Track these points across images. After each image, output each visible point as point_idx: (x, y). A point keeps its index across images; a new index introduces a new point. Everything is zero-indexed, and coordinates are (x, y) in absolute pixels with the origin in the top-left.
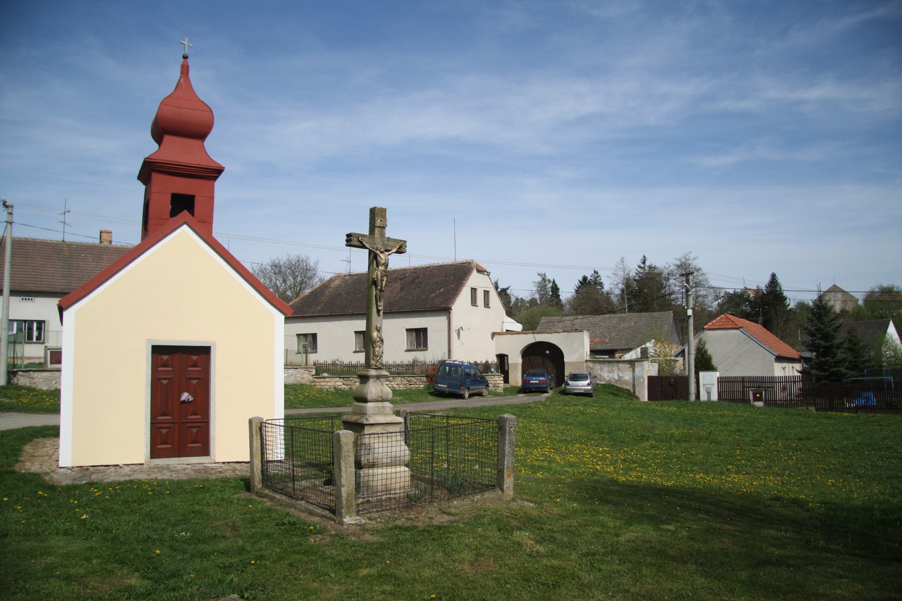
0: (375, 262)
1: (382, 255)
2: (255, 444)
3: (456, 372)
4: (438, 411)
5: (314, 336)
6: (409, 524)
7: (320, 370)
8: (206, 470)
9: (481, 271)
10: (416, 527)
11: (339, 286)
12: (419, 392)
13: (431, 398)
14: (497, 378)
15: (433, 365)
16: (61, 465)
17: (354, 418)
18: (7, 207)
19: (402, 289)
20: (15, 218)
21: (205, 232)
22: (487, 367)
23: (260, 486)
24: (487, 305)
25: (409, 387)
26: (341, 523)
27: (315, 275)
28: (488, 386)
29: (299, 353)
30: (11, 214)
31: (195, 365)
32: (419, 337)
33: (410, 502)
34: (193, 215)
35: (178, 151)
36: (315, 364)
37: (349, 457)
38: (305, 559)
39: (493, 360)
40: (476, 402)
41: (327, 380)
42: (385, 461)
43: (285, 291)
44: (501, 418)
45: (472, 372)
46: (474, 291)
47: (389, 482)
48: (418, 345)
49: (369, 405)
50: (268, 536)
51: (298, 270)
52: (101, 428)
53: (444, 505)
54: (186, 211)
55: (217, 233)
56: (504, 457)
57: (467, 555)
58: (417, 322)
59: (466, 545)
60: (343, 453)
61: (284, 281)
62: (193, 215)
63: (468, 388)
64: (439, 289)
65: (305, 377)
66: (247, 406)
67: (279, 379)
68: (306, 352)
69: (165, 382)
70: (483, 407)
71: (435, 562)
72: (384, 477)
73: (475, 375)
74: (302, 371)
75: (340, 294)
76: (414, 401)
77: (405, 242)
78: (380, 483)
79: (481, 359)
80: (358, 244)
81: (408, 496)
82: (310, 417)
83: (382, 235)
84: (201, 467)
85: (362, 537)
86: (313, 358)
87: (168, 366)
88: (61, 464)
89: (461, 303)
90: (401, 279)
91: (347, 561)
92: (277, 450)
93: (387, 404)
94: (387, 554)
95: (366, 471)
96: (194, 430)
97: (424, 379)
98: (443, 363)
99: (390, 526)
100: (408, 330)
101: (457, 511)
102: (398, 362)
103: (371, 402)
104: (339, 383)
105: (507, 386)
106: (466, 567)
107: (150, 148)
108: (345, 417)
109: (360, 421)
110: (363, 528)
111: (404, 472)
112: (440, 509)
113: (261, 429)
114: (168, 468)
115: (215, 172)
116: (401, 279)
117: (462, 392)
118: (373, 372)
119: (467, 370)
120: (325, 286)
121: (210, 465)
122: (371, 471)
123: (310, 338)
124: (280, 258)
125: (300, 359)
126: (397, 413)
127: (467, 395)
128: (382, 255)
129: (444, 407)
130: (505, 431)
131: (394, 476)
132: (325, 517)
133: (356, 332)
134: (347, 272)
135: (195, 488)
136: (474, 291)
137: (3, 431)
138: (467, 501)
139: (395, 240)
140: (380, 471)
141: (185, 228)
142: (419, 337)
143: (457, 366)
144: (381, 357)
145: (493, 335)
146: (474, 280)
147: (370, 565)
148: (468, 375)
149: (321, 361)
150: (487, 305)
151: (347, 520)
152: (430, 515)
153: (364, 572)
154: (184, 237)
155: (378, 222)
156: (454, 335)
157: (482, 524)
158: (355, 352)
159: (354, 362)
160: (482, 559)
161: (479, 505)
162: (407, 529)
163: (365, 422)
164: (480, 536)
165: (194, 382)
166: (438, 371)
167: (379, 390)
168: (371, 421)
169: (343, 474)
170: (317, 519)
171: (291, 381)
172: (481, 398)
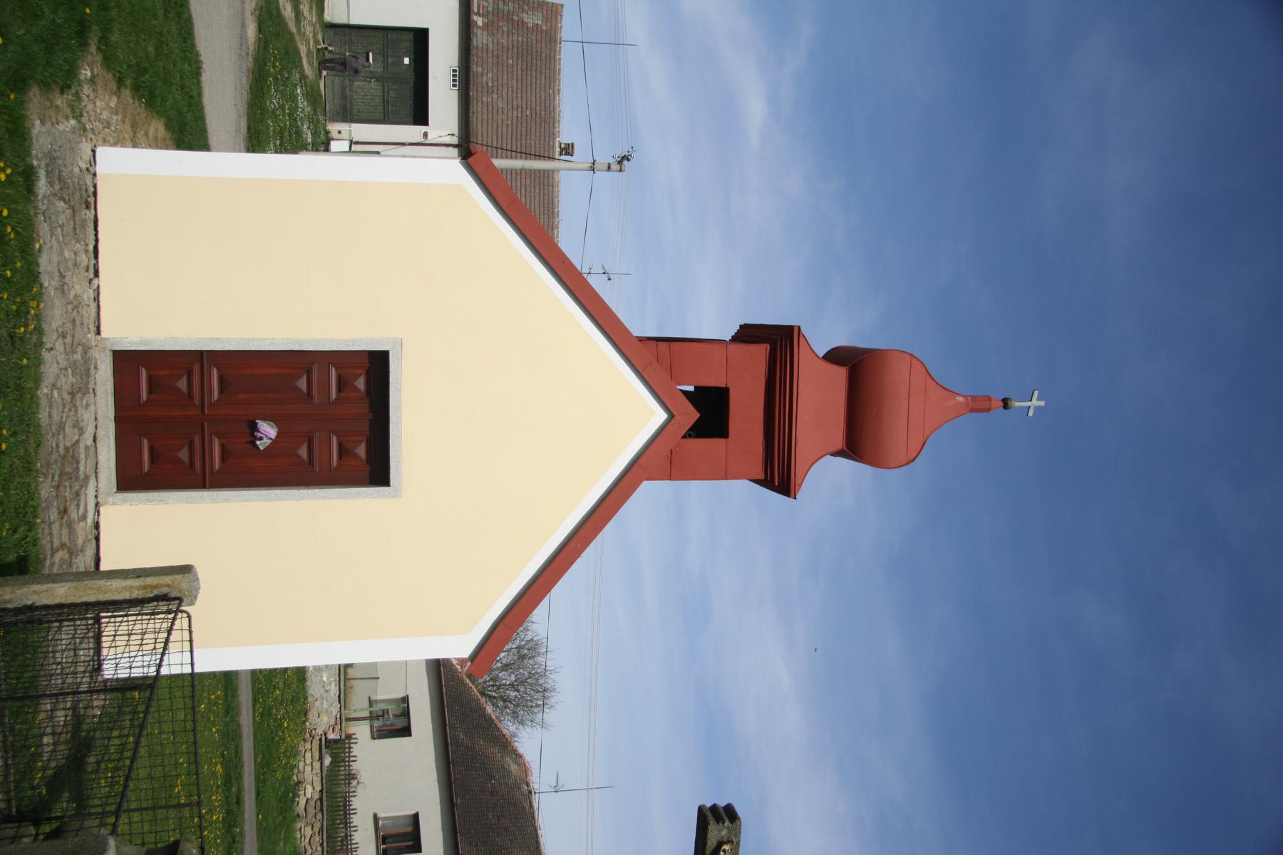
5: (406, 731)
7: (338, 749)
8: (72, 475)
11: (507, 773)
16: (100, 150)
18: (620, 163)
20: (600, 175)
21: (652, 463)
27: (522, 723)
29: (371, 703)
30: (609, 168)
31: (343, 451)
34: (684, 437)
35: (819, 399)
36: (349, 737)
41: (317, 765)
51: (529, 693)
52: (189, 242)
54: (696, 415)
55: (650, 492)
62: (684, 437)
65: (322, 717)
66: (254, 586)
68: (372, 717)
69: (302, 384)
75: (491, 777)
82: (232, 735)
86: (362, 731)
87: (339, 390)
88: (102, 152)
92: (127, 653)
96: (184, 454)
103: (364, 719)
104: (310, 790)
107: (822, 336)
114: (83, 388)
115: (779, 476)
120: (505, 745)
121: (91, 491)
123: (400, 723)
125: (359, 706)
133: (416, 816)
134: (535, 786)
141: (660, 416)
149: (356, 750)
154: (640, 415)
158: (376, 818)
159: (356, 820)
165: (303, 452)
171: (314, 689)
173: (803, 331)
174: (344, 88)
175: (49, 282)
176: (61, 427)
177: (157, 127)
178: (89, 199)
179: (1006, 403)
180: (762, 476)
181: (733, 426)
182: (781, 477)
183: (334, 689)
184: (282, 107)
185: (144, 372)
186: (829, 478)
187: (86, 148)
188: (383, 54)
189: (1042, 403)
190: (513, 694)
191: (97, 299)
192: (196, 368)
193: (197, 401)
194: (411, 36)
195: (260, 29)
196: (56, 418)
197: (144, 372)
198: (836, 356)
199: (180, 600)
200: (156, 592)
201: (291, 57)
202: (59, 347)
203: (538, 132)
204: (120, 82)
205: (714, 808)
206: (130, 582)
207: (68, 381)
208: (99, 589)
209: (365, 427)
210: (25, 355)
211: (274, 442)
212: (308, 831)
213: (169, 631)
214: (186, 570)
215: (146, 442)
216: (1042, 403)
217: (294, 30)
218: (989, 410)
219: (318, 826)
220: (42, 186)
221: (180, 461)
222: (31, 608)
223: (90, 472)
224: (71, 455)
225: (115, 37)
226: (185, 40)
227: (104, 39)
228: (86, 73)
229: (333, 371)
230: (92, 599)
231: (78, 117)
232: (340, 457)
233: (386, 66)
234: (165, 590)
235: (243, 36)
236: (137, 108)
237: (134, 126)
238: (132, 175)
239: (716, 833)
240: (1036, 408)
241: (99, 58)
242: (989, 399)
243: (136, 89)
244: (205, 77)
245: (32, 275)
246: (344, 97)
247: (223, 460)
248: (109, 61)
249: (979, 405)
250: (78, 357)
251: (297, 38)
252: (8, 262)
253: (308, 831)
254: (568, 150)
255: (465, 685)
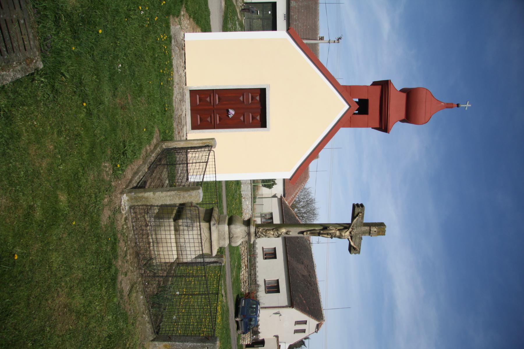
0: (342, 228)
1: (348, 233)
2: (196, 142)
3: (252, 312)
4: (226, 299)
6: (120, 252)
9: (318, 327)
10: (116, 257)
12: (239, 288)
13: (235, 295)
14: (249, 339)
15: (256, 297)
16: (186, 34)
17: (215, 214)
18: (338, 40)
19: (303, 276)
20: (332, 45)
21: (345, 122)
22: (256, 333)
23: (164, 147)
24: (296, 331)
25: (242, 282)
26: (122, 193)
28: (244, 333)
30: (334, 42)
32: (273, 288)
33: (145, 261)
35: (397, 105)
37: (179, 199)
38: (85, 150)
39: (261, 337)
40: (233, 326)
42: (182, 240)
43: (297, 208)
44: (216, 338)
45: (252, 323)
46: (305, 322)
47: (165, 245)
48: (269, 288)
49: (226, 227)
50: (114, 130)
52: (211, 58)
53: (139, 287)
55: (343, 131)
56: (182, 342)
57: (78, 301)
58: (283, 286)
59: (90, 302)
60: (182, 193)
61: (303, 207)
63: (242, 320)
64: (305, 300)
67: (245, 175)
69: (241, 98)
70: (230, 330)
71: (71, 268)
72: (169, 241)
73: (250, 324)
74: (250, 213)
76: (233, 285)
77: (359, 252)
78: (163, 236)
79: (261, 329)
80: (356, 213)
81: (151, 259)
83: (364, 233)
84: (183, 122)
85: (107, 208)
87: (252, 100)
88: (187, 35)
89: (296, 314)
90: (309, 275)
91: (80, 186)
93: (227, 242)
94: (85, 225)
95: (172, 224)
96: (209, 119)
97: (247, 292)
98: (258, 303)
99: (119, 236)
100: (278, 280)
101: (133, 298)
102: (258, 274)
105: (244, 347)
106: (63, 299)
107: (398, 84)
108: (216, 210)
109: (213, 219)
110: (117, 210)
111: (172, 256)
112: (135, 283)
113: (208, 146)
114: (182, 100)
116: (309, 275)
117: (239, 316)
118: (253, 229)
119: (254, 319)
122: (172, 228)
124: (316, 204)
126: (221, 250)
127: (237, 319)
128: (348, 233)
129: (229, 303)
130: (205, 342)
131: (169, 249)
132: (131, 181)
133: (275, 248)
135: (165, 104)
136: (305, 322)
137: (206, 4)
138: (142, 308)
139: (360, 244)
140: (173, 237)
141: (347, 107)
142: (273, 288)
143: (256, 312)
144: (265, 236)
145: (277, 337)
146: (312, 323)
147: (71, 205)
148: (251, 320)
150: (296, 331)
151: (125, 198)
152: (129, 274)
153: (63, 198)
154: (341, 107)
155: (374, 229)
156: (276, 310)
157: (117, 320)
158: (263, 248)
160: (74, 317)
161: (140, 318)
162: (114, 249)
163: (212, 223)
164: (103, 318)
165: (242, 118)
166: (253, 300)
167: (238, 235)
168: (213, 228)
169: (164, 194)
170: (129, 176)
172: (236, 329)
173: (392, 81)
174: (250, 22)
175: (175, 69)
176: (178, 109)
177: (199, 29)
178: (183, 48)
179: (458, 105)
180: (378, 126)
181: (370, 111)
182: (385, 128)
183: (250, 206)
184: (232, 27)
185: (198, 96)
186: (399, 128)
187: (182, 33)
188: (262, 11)
189: (470, 105)
190: (305, 215)
191: (185, 76)
192: (212, 95)
193: (212, 104)
194: (271, 5)
195: (226, 4)
196: (177, 106)
197: (198, 96)
198: (403, 91)
199: (212, 146)
200: (205, 144)
201: (234, 12)
202: (177, 86)
203: (312, 31)
204: (190, 16)
205: (357, 205)
206: (199, 142)
207: (179, 97)
208: (191, 143)
209: (259, 111)
210: (170, 86)
211: (234, 115)
212: (243, 248)
213: (209, 155)
214: (213, 139)
215: (199, 116)
216: (470, 105)
217: (235, 4)
218: (452, 107)
219: (246, 247)
220: (173, 41)
221: (208, 121)
222: (175, 148)
223: (185, 124)
224: (180, 117)
225: (189, 3)
226: (206, 5)
227: (186, 4)
228: (182, 13)
229: (250, 95)
230: (190, 146)
231: (180, 25)
232: (252, 120)
233: (263, 14)
234: (208, 144)
235: (221, 6)
236: (194, 24)
237: (193, 29)
238: (194, 41)
239: (357, 210)
240: (468, 107)
241: (185, 9)
242: (452, 104)
243: (194, 18)
244: (211, 17)
245: (171, 65)
246: (250, 25)
247: (220, 121)
248: (187, 10)
249: (449, 106)
250: (181, 91)
251: (236, 7)
252: (166, 61)
253: (243, 248)
254: (322, 39)
255: (290, 210)
